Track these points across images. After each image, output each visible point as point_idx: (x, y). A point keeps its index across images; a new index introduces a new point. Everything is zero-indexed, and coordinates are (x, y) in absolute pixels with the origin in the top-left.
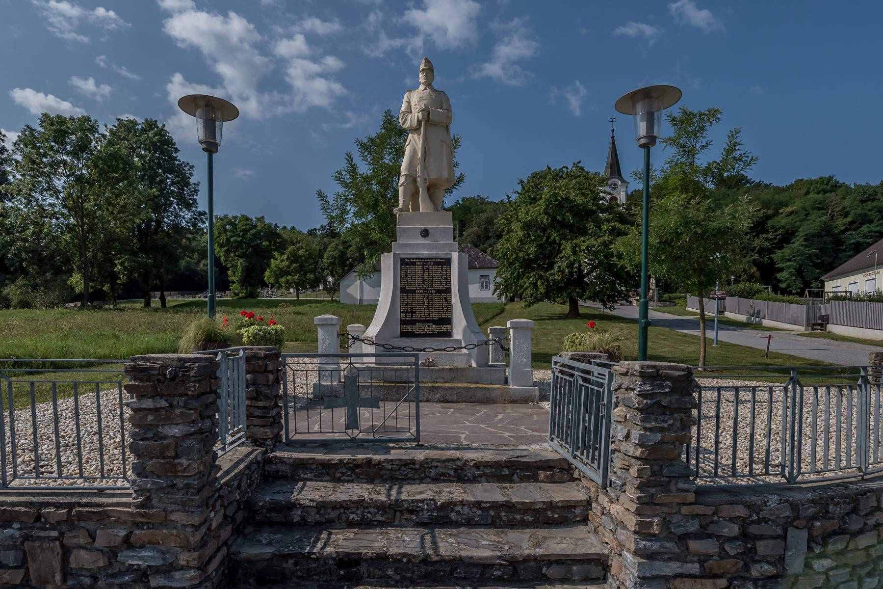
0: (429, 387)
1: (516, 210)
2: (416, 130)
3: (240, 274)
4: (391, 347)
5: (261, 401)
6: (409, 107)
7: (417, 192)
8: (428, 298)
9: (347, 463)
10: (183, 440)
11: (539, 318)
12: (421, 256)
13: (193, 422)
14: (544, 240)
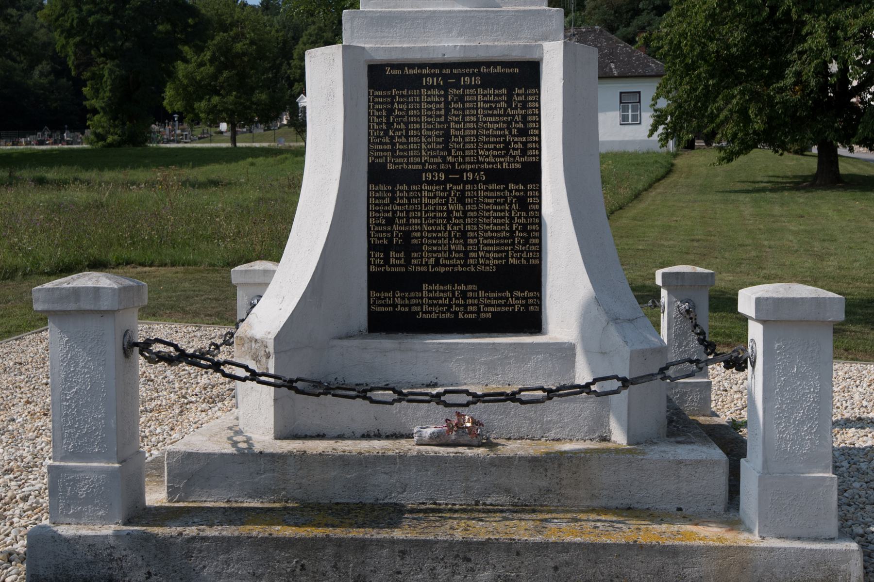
0: (451, 545)
3: (108, 94)
8: (461, 200)
11: (750, 187)
14: (765, 14)
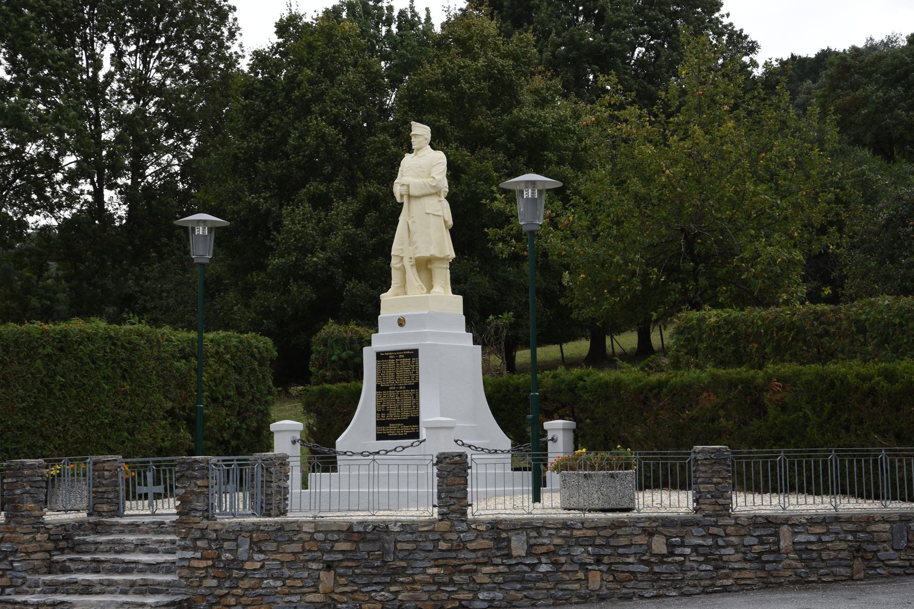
8: (399, 396)
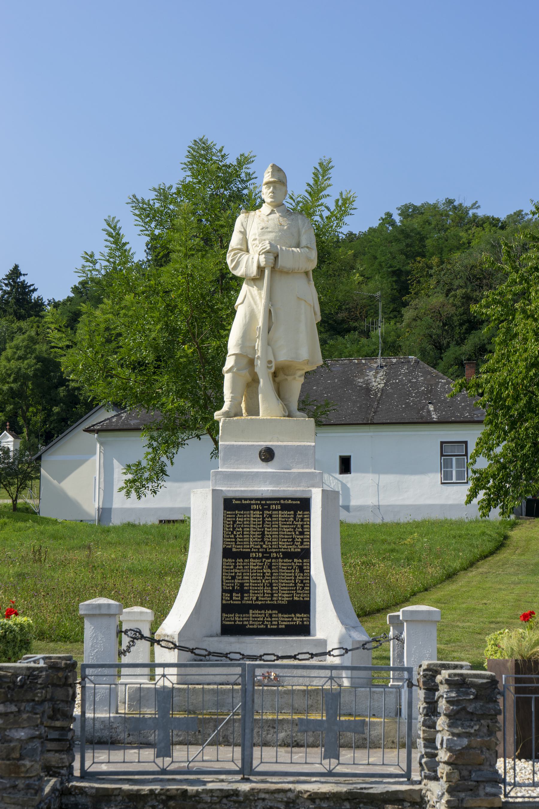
1: (527, 281)
2: (257, 280)
4: (204, 653)
5: (58, 720)
6: (245, 241)
7: (255, 380)
8: (270, 567)
9: (160, 794)
10: (27, 743)
12: (259, 495)
13: (37, 726)
